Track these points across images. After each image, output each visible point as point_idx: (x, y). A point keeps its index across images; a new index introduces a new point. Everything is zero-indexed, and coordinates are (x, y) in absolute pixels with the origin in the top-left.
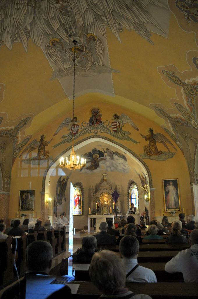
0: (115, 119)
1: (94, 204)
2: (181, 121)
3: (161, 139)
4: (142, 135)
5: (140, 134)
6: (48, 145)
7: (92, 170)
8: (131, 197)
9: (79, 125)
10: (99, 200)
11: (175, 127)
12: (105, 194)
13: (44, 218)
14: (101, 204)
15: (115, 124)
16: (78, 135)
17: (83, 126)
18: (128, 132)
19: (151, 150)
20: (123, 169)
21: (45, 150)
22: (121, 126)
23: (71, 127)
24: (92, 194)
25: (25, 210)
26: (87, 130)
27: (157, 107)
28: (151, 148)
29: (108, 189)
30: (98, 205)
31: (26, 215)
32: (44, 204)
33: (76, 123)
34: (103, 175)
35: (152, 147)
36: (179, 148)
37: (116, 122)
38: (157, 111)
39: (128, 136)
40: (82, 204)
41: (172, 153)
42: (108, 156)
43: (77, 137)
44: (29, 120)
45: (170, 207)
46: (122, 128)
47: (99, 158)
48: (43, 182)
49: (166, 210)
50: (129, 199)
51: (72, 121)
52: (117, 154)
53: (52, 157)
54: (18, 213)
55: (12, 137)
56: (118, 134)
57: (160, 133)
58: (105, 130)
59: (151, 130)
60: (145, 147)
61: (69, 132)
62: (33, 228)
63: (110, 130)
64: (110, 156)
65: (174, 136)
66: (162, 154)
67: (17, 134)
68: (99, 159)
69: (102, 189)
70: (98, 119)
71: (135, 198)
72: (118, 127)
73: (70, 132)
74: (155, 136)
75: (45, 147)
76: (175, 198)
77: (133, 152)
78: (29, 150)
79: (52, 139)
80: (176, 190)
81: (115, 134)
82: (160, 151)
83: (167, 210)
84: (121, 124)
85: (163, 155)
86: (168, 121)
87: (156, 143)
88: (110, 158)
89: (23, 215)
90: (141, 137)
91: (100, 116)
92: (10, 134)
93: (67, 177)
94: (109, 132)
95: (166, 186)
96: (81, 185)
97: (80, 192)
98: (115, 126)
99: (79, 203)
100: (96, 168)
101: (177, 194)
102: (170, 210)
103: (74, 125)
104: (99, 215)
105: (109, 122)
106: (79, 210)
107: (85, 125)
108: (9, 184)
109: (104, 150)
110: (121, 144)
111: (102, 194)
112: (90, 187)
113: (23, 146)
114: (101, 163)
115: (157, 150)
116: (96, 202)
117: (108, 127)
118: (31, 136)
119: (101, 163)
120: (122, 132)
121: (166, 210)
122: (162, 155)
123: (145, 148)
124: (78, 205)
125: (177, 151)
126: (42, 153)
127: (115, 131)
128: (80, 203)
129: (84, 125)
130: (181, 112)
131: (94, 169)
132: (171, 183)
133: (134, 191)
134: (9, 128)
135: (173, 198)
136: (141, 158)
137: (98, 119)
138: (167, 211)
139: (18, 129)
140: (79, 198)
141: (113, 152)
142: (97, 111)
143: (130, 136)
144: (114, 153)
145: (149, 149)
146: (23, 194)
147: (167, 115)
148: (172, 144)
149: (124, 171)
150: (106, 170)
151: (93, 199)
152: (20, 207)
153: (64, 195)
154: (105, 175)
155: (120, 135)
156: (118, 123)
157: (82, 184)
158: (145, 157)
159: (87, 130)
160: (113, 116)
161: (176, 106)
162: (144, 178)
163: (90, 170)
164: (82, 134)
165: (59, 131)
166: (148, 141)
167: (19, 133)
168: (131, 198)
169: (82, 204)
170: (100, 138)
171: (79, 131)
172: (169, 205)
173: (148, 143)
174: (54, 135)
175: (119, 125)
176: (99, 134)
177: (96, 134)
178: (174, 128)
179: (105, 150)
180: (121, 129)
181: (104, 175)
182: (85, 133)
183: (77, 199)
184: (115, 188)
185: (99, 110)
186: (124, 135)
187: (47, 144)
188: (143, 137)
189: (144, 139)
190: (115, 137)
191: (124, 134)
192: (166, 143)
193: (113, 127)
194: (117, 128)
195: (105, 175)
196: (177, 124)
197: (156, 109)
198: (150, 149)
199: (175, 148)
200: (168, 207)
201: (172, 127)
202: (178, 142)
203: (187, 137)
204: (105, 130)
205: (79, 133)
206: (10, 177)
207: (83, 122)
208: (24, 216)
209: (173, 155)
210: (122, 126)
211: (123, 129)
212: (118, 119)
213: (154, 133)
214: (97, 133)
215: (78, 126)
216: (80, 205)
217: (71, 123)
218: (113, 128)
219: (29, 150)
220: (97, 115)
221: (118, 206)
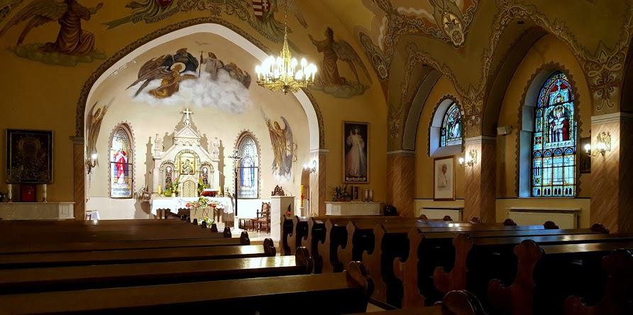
2: (423, 24)
16: (172, 7)
21: (80, 30)
22: (271, 10)
36: (379, 76)
41: (363, 87)
42: (206, 71)
46: (275, 13)
47: (184, 72)
52: (229, 71)
56: (264, 26)
57: (346, 42)
58: (238, 10)
59: (330, 32)
64: (211, 72)
68: (182, 75)
72: (266, 10)
74: (337, 46)
75: (82, 20)
79: (101, 5)
82: (342, 78)
86: (385, 19)
88: (208, 77)
93: (105, 107)
98: (260, 7)
100: (169, 95)
106: (125, 186)
109: (201, 57)
114: (184, 86)
115: (338, 75)
119: (185, 86)
124: (122, 175)
125: (372, 83)
126: (73, 35)
130: (434, 6)
131: (165, 97)
141: (222, 63)
144: (223, 67)
148: (364, 68)
150: (193, 102)
155: (268, 28)
162: (279, 128)
170: (225, 26)
179: (206, 56)
180: (272, 16)
182: (191, 8)
183: (120, 160)
186: (277, 32)
190: (259, 31)
193: (255, 6)
194: (262, 10)
196: (405, 29)
211: (276, 16)
214: (218, 13)
218: (256, 10)
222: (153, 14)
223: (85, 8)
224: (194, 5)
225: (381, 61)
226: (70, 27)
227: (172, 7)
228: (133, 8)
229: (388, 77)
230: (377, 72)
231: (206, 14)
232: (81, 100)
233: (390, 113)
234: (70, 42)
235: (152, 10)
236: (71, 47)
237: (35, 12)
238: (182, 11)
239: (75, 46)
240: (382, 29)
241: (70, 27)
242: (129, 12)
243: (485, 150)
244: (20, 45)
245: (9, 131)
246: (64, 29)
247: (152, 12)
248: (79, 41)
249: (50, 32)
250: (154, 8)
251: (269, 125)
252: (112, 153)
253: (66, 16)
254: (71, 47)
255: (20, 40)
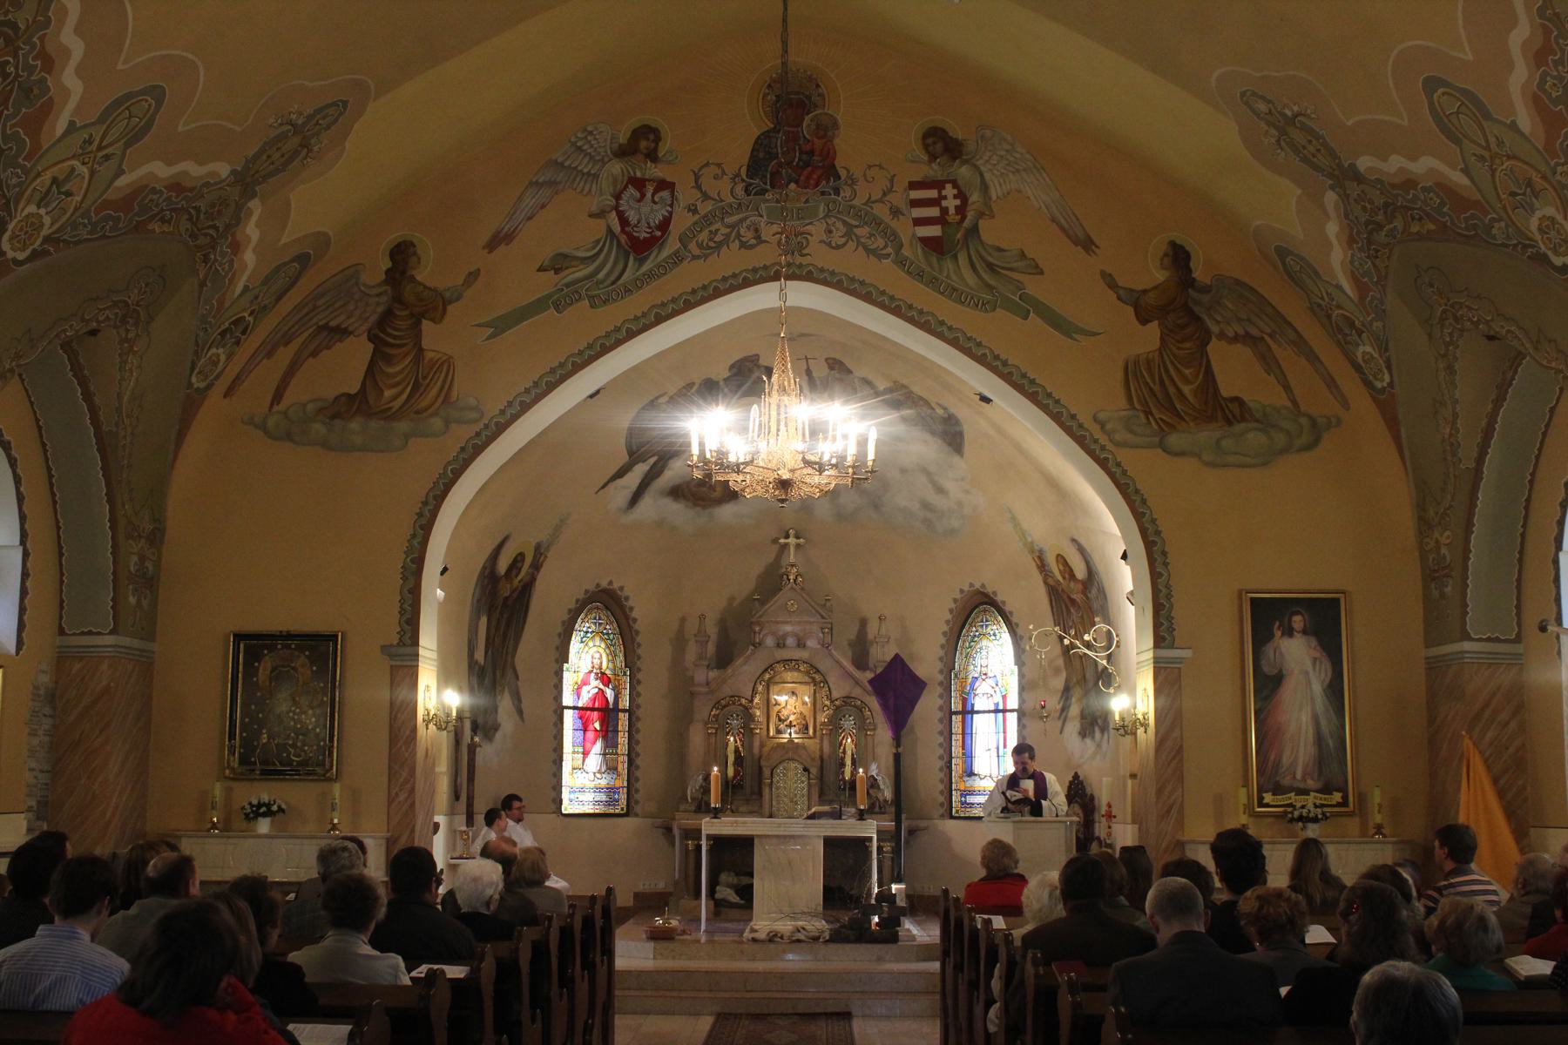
0: (933, 157)
1: (713, 740)
2: (1443, 204)
3: (1240, 320)
4: (1112, 284)
5: (1103, 274)
6: (441, 321)
7: (704, 507)
8: (965, 701)
9: (677, 187)
10: (748, 717)
11: (1369, 242)
12: (789, 676)
13: (413, 831)
14: (762, 745)
15: (933, 194)
16: (665, 253)
17: (706, 197)
18: (1023, 255)
19: (1172, 390)
20: (926, 506)
21: (421, 350)
22: (970, 215)
23: (618, 197)
24: (701, 676)
25: (270, 774)
26: (733, 226)
27: (1263, 98)
28: (1172, 380)
29: (811, 643)
30: (737, 751)
31: (280, 810)
32: (414, 729)
33: (655, 171)
34: (775, 541)
35: (1179, 372)
36: (1368, 384)
37: (938, 185)
38: (1263, 126)
39: (1019, 286)
40: (623, 739)
41: (1314, 423)
43: (659, 266)
44: (336, 120)
45: (1286, 781)
46: (981, 223)
48: (405, 578)
49: (1261, 799)
50: (952, 713)
51: (623, 152)
53: (473, 402)
54: (218, 790)
55: (202, 241)
56: (949, 264)
57: (1238, 282)
58: (862, 232)
59: (1179, 257)
60: (1136, 363)
61: (604, 229)
62: (488, 904)
63: (893, 237)
65: (1339, 307)
66: (1243, 419)
67: (238, 219)
69: (770, 641)
70: (812, 153)
71: (996, 711)
72: (952, 216)
73: (610, 231)
74: (1205, 298)
75: (426, 325)
76: (1323, 722)
77: (1049, 395)
78: (300, 340)
79: (473, 276)
80: (1326, 666)
81: (931, 266)
83: (1268, 798)
84: (974, 197)
85: (1256, 425)
86: (1331, 198)
87: (1204, 343)
89: (260, 805)
90: (1112, 295)
91: (826, 129)
92: (190, 219)
93: (538, 548)
94: (889, 250)
95: (1262, 638)
96: (622, 607)
97: (613, 656)
98: (934, 212)
99: (608, 734)
101: (1334, 690)
102: (1282, 799)
103: (639, 184)
104: (743, 814)
105: (892, 181)
107: (722, 189)
108: (149, 582)
110: (970, 339)
111: (768, 678)
112: (683, 620)
113: (260, 312)
115: (1216, 390)
116: (722, 729)
117: (881, 211)
118: (322, 242)
120: (978, 251)
121: (1261, 799)
122: (1243, 425)
123: (1133, 372)
124: (598, 747)
125: (1345, 404)
127: (928, 243)
128: (616, 731)
129: (708, 183)
132: (1298, 622)
133: (991, 662)
134: (195, 170)
135: (1305, 718)
136: (1103, 440)
137: (812, 153)
138: (1267, 805)
139: (247, 181)
140: (609, 694)
142: (809, 98)
143: (1033, 287)
145: (1162, 382)
146: (253, 656)
147: (1333, 155)
148: (1313, 358)
149: (927, 523)
151: (703, 710)
152: (232, 752)
153: (509, 673)
154: (792, 540)
155: (961, 272)
156: (949, 191)
157: (630, 603)
158: (1132, 432)
159: (729, 220)
160: (920, 136)
161: (1431, 104)
162: (1072, 576)
163: (696, 505)
164: (692, 246)
165: (530, 218)
166: (1154, 329)
167: (250, 213)
168: (968, 712)
169: (623, 739)
170: (825, 283)
171: (676, 229)
172: (1277, 764)
173: (1158, 344)
174: (492, 245)
175: (958, 202)
176: (818, 255)
177: (799, 260)
178: (1361, 249)
180: (974, 230)
181: (786, 545)
182: (719, 245)
183: (594, 699)
184: (852, 633)
185: (823, 89)
187: (435, 306)
188: (1119, 298)
189: (1130, 310)
190: (933, 283)
191: (991, 267)
192: (1273, 346)
194: (941, 220)
195: (792, 540)
196: (1398, 223)
197: (1257, 113)
198: (1167, 382)
199: (1337, 386)
200: (1271, 780)
201: (1351, 241)
202: (1365, 349)
203: (1457, 319)
204: (858, 231)
205: (672, 245)
206: (156, 537)
207: (707, 164)
208: (269, 813)
209: (1317, 431)
210: (981, 215)
211: (990, 232)
212: (954, 159)
213: (1199, 273)
214: (801, 249)
215: (665, 194)
216: (615, 745)
217: (616, 168)
218: (919, 222)
219: (300, 340)
220: (807, 119)
221: (874, 759)
222: (612, 278)
223: (435, 290)
224: (728, 236)
225: (1360, 333)
226: (393, 346)
227: (665, 253)
228: (557, 271)
229: (1391, 384)
230: (1358, 368)
231: (766, 255)
232: (415, 542)
233: (1421, 507)
234: (393, 386)
235: (608, 266)
236: (394, 398)
237: (314, 321)
238: (695, 257)
239: (405, 396)
240: (1332, 228)
241: (393, 346)
242: (548, 282)
243: (1160, 678)
244: (276, 408)
245: (239, 637)
246: (381, 354)
247: (608, 275)
248: (416, 380)
249: (353, 359)
250: (615, 263)
251: (1042, 566)
252: (569, 680)
253: (387, 318)
254: (394, 398)
255: (278, 397)
